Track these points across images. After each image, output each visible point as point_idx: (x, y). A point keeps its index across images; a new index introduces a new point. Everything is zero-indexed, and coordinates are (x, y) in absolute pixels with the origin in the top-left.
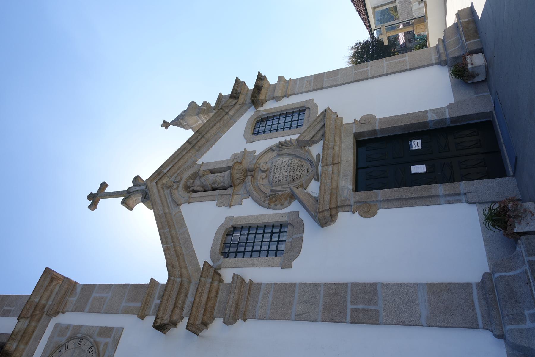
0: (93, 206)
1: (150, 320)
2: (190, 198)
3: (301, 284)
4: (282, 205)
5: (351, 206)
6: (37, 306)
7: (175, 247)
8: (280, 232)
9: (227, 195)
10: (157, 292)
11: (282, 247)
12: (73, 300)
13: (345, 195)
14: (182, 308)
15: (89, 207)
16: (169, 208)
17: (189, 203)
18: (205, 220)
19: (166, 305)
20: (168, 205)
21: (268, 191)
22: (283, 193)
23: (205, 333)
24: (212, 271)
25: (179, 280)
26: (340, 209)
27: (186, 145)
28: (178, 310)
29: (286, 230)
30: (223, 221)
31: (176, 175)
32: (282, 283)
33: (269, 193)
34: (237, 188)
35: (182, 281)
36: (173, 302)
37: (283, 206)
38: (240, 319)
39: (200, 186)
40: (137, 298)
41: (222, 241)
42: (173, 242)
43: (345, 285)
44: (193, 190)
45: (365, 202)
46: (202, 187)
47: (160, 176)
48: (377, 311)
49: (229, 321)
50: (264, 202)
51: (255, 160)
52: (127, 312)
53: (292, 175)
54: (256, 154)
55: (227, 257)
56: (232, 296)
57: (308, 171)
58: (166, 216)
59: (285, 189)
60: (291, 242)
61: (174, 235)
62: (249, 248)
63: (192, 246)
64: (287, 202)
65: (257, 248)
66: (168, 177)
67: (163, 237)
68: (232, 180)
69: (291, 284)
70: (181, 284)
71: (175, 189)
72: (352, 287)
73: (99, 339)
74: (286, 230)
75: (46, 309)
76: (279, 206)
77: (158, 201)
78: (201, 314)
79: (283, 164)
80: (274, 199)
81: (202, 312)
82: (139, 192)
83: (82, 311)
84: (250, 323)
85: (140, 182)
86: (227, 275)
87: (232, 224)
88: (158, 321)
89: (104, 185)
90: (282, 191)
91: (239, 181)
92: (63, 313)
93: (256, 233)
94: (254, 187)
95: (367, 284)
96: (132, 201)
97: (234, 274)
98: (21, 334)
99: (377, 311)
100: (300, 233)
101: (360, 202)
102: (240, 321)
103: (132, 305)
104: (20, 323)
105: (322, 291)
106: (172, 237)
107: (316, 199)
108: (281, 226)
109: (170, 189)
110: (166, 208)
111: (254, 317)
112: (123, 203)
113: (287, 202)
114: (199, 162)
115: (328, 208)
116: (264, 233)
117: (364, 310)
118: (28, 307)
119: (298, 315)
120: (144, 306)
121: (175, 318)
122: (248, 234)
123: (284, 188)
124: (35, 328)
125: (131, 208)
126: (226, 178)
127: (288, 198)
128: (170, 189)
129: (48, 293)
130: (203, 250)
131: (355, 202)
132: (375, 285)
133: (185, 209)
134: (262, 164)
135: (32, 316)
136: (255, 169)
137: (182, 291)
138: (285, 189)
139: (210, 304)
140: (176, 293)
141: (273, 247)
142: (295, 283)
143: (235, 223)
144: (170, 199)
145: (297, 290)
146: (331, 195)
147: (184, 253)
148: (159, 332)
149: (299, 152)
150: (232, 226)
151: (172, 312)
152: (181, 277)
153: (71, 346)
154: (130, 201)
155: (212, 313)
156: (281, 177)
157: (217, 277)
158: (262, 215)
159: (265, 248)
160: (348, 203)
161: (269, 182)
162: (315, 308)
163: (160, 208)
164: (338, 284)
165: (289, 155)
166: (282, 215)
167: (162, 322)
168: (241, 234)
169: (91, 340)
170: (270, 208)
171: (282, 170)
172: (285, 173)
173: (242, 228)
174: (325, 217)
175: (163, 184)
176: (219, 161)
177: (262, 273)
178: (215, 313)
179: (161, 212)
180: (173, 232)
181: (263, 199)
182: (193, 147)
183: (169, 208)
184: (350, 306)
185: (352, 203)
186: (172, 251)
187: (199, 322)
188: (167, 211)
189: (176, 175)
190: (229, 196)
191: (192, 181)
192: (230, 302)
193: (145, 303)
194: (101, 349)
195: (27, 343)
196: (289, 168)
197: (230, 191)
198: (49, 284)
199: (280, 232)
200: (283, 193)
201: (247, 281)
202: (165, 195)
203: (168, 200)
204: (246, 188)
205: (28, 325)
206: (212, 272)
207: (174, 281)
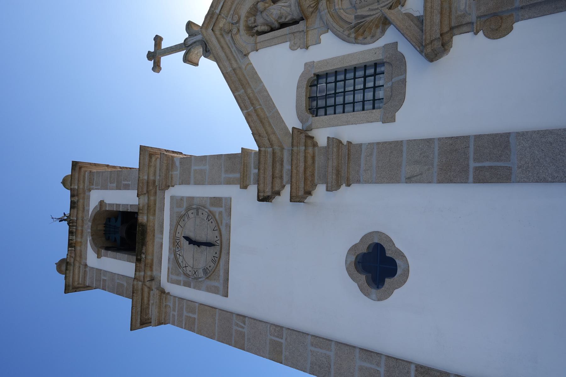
0: (157, 67)
1: (253, 190)
2: (256, 43)
3: (409, 142)
4: (373, 36)
5: (472, 23)
6: (148, 182)
7: (256, 110)
8: (375, 74)
9: (300, 32)
10: (252, 161)
11: (380, 94)
12: (176, 173)
13: (462, 7)
14: (281, 177)
15: (154, 69)
16: (236, 61)
17: (257, 50)
18: (282, 67)
19: (264, 177)
20: (234, 57)
21: (351, 18)
22: (372, 18)
23: (309, 199)
24: (303, 136)
25: (270, 150)
26: (455, 31)
28: (277, 181)
29: (383, 69)
30: (301, 69)
31: (232, 12)
32: (386, 142)
33: (354, 22)
35: (273, 150)
37: (374, 38)
38: (344, 185)
39: (264, 24)
40: (234, 167)
41: (306, 96)
42: (253, 104)
43: (465, 139)
44: (257, 31)
45: (495, 15)
46: (267, 25)
47: (214, 20)
48: (509, 169)
49: (333, 187)
50: (349, 36)
52: (229, 182)
55: (316, 116)
56: (330, 163)
58: (235, 73)
59: (374, 12)
60: (392, 87)
61: (251, 95)
62: (340, 100)
63: (275, 106)
64: (379, 30)
65: (349, 98)
66: (223, 18)
67: (240, 101)
68: (302, 11)
69: (397, 142)
70: (274, 153)
71: (236, 34)
72: (475, 141)
73: (213, 209)
74: (383, 69)
75: (157, 184)
76: (369, 38)
77: (222, 54)
78: (302, 185)
80: (361, 30)
81: (303, 183)
82: (198, 43)
83: (188, 183)
84: (355, 188)
85: (195, 29)
86: (322, 136)
87: (313, 72)
88: (261, 194)
89: (158, 40)
91: (311, 10)
92: (173, 186)
93: (345, 80)
94: (332, 16)
95: (496, 135)
96: (194, 56)
97: (328, 138)
98: (146, 207)
99: (509, 169)
100: (401, 75)
101: (485, 16)
102: (343, 187)
103: (231, 176)
104: (141, 200)
105: (436, 149)
106: (249, 98)
107: (420, 21)
108: (376, 65)
109: (230, 35)
110: (233, 62)
111: (358, 182)
112: (186, 59)
113: (379, 30)
115: (439, 36)
116: (355, 78)
117: (491, 167)
118: (141, 185)
119: (409, 178)
120: (243, 177)
121: (277, 189)
122: (336, 82)
123: (372, 10)
124: (155, 201)
125: (196, 64)
126: (293, 8)
127: (381, 25)
128: (230, 35)
129: (152, 169)
130: (290, 116)
131: (479, 17)
132: (508, 135)
133: (253, 57)
135: (148, 192)
137: (276, 160)
138: (374, 12)
139: (308, 173)
140: (271, 164)
141: (369, 95)
142: (402, 141)
143: (317, 71)
144: (234, 48)
145: (405, 149)
146: (441, 13)
147: (268, 115)
148: (265, 202)
150: (314, 74)
151: (272, 183)
152: (272, 145)
153: (191, 216)
154: (192, 56)
155: (313, 181)
157: (309, 142)
158: (349, 55)
159: (359, 97)
160: (468, 19)
161: (351, 4)
162: (429, 169)
163: (227, 64)
164: (457, 138)
166: (375, 50)
167: (265, 195)
168: (327, 83)
169: (206, 210)
170: (358, 43)
173: (327, 75)
174: (434, 48)
175: (221, 29)
177: (360, 131)
178: (316, 181)
179: (229, 69)
180: (249, 91)
181: (346, 33)
183: (236, 61)
184: (472, 164)
185: (473, 18)
186: (255, 117)
187: (301, 193)
188: (235, 66)
189: (232, 12)
190: (302, 33)
191: (252, 19)
192: (330, 169)
193: (244, 174)
194: (217, 216)
195: (154, 214)
197: (301, 26)
198: (150, 161)
199: (375, 74)
200: (372, 18)
201: (345, 143)
202: (227, 44)
203: (233, 50)
204: (321, 18)
205: (148, 200)
206: (304, 136)
207: (265, 152)
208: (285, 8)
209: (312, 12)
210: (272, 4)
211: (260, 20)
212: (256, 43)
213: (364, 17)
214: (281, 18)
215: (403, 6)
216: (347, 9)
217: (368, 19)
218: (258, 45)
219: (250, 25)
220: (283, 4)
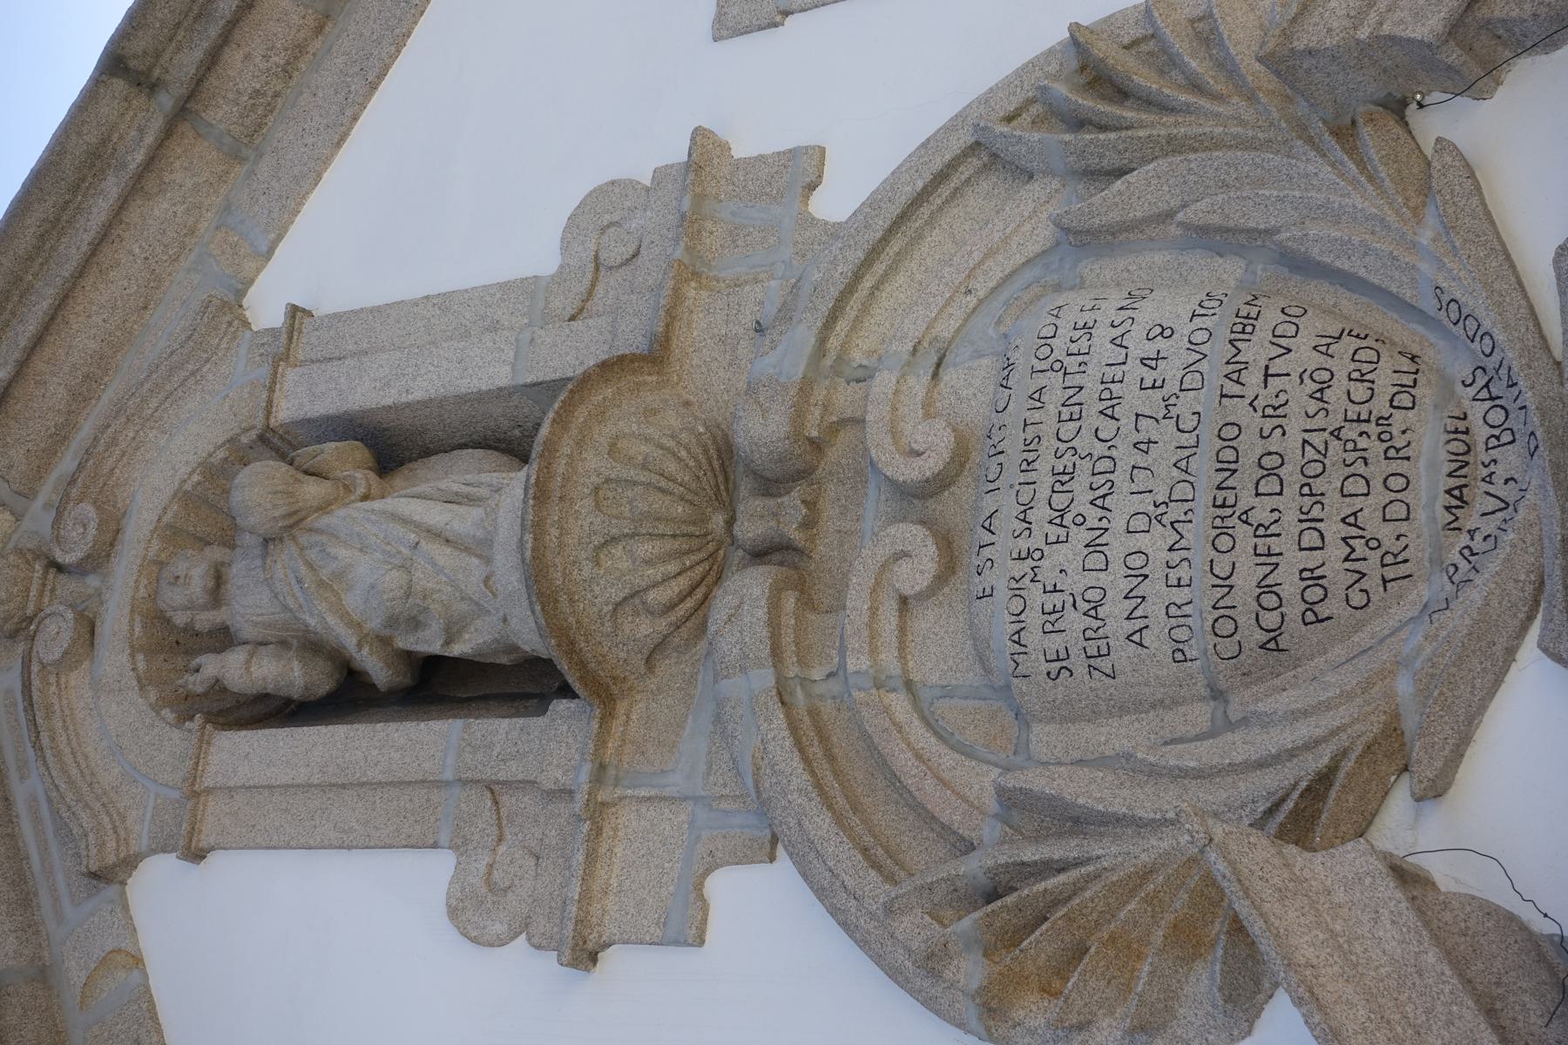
17: (197, 855)
27: (108, 109)
34: (635, 712)
36: (1318, 732)
44: (218, 688)
51: (804, 334)
53: (1248, 576)
54: (836, 201)
57: (1458, 498)
71: (68, 661)
79: (1133, 399)
80: (1041, 945)
90: (1140, 825)
91: (645, 628)
109: (20, 648)
114: (266, 306)
128: (20, 648)
134: (884, 382)
136: (817, 446)
149: (1320, 199)
156: (1114, 609)
165: (1215, 238)
171: (1123, 505)
172: (1156, 542)
176: (443, 302)
182: (183, 112)
196: (1203, 465)
197: (550, 742)
208: (444, 555)
209: (655, 652)
210: (363, 478)
211: (250, 605)
212: (195, 793)
213: (1078, 821)
214: (415, 623)
215: (1434, 790)
216: (947, 692)
217: (1109, 851)
218: (214, 808)
219: (180, 619)
220: (436, 515)
